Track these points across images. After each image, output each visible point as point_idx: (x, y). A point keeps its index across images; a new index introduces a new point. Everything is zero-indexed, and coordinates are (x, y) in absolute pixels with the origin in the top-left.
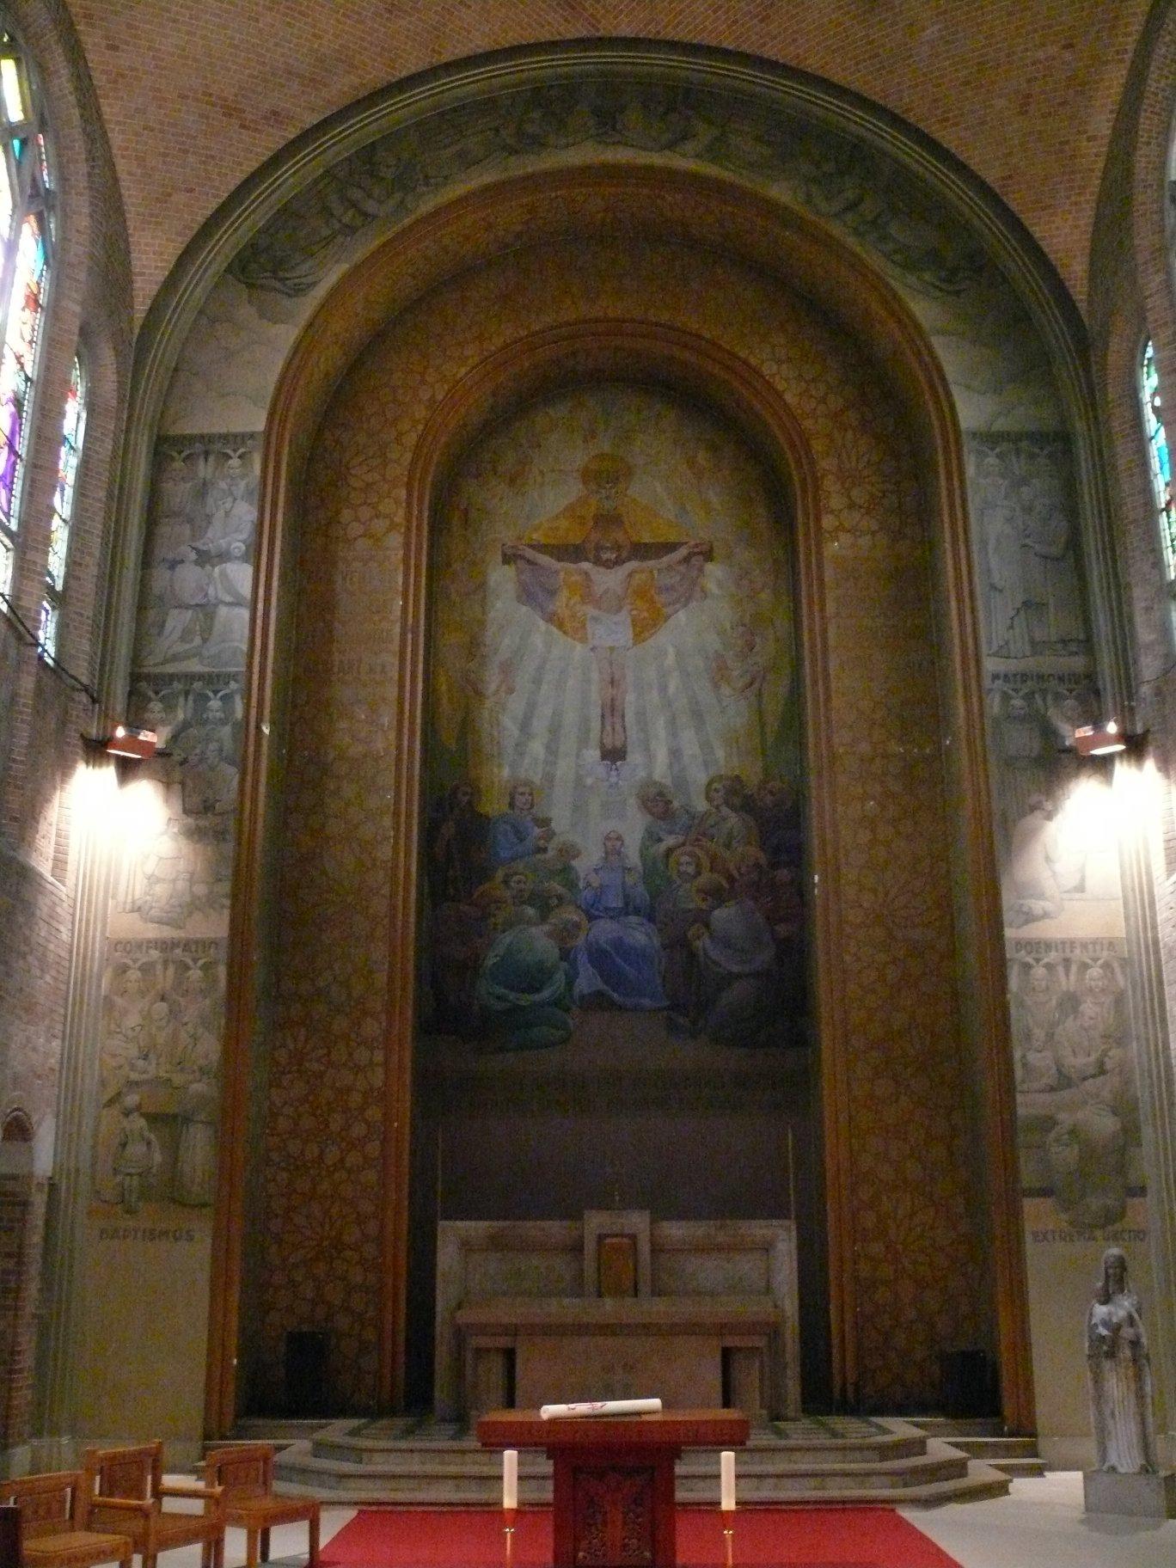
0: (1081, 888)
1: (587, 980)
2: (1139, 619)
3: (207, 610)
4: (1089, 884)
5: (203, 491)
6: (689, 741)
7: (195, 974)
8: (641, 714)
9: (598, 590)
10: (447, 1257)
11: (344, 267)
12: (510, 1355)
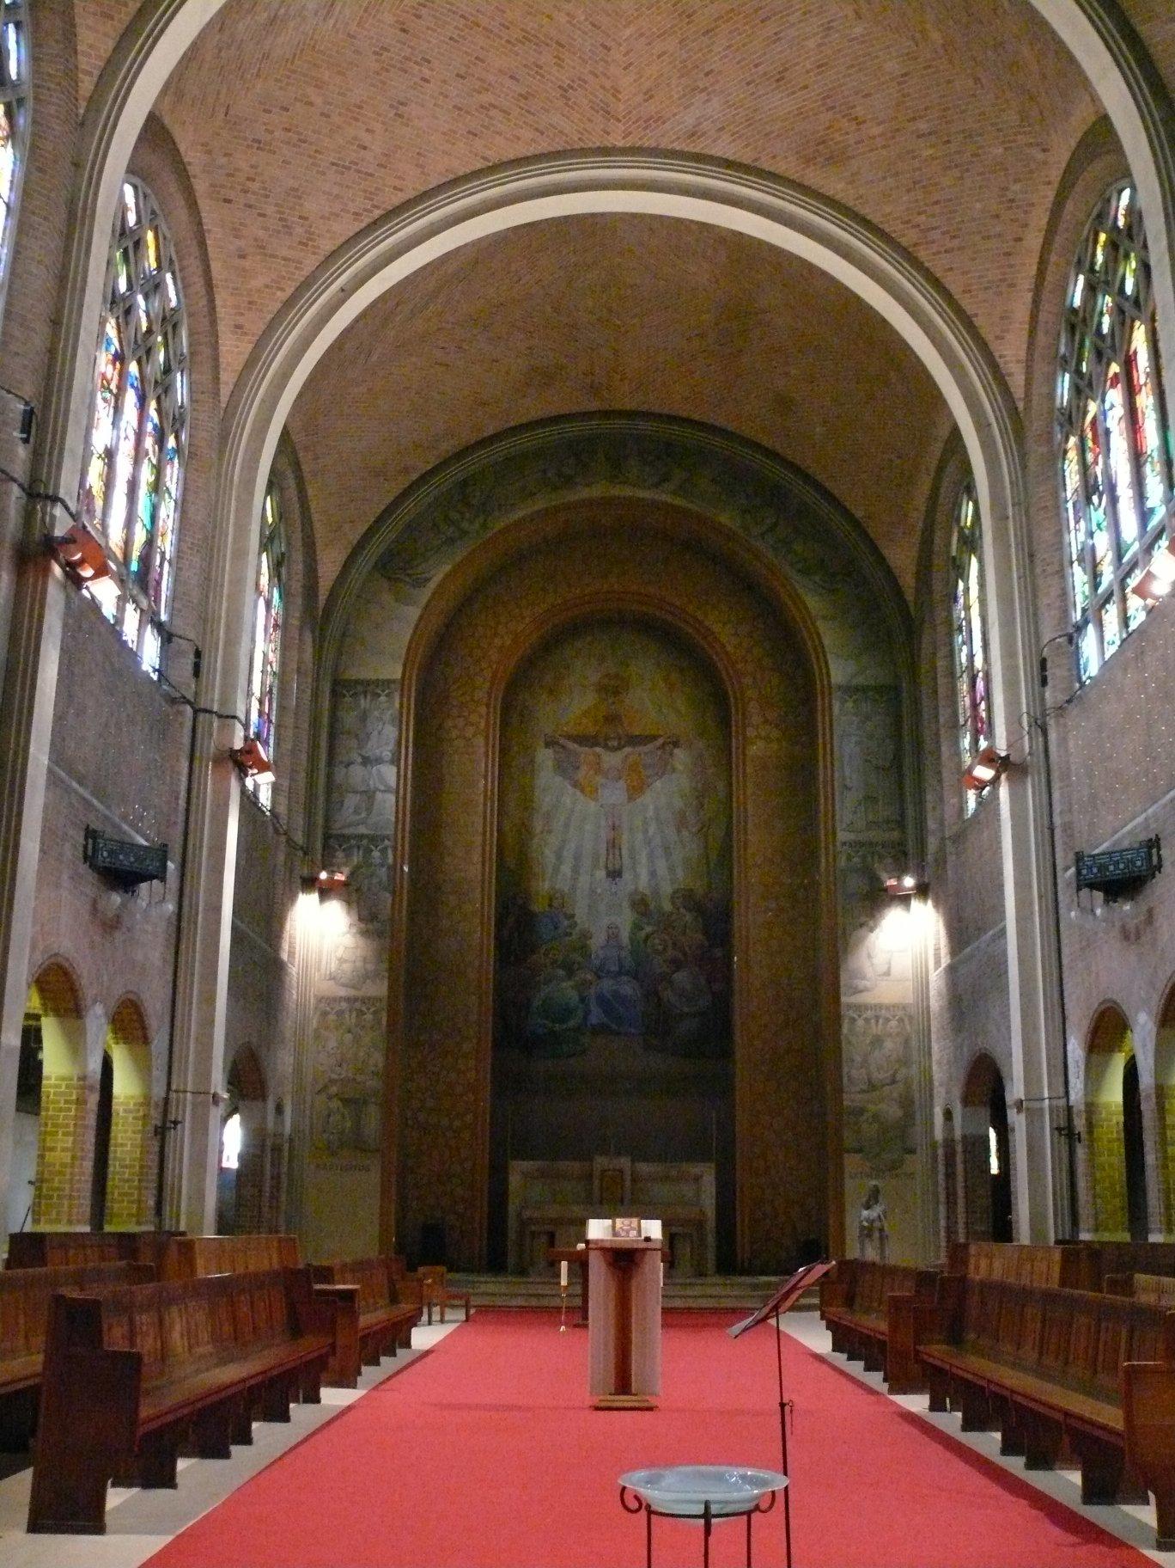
0: (888, 973)
1: (596, 1016)
2: (929, 815)
3: (369, 795)
4: (893, 971)
5: (364, 718)
6: (661, 866)
7: (369, 1017)
8: (632, 850)
9: (605, 766)
10: (515, 1181)
11: (448, 568)
12: (552, 1237)
